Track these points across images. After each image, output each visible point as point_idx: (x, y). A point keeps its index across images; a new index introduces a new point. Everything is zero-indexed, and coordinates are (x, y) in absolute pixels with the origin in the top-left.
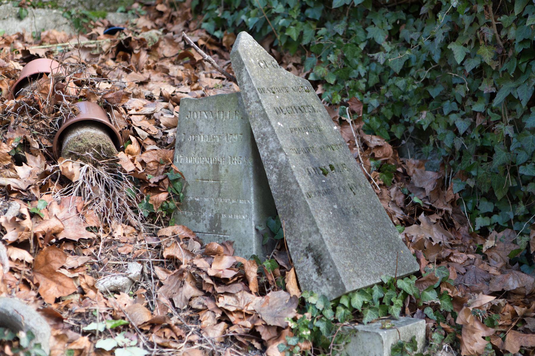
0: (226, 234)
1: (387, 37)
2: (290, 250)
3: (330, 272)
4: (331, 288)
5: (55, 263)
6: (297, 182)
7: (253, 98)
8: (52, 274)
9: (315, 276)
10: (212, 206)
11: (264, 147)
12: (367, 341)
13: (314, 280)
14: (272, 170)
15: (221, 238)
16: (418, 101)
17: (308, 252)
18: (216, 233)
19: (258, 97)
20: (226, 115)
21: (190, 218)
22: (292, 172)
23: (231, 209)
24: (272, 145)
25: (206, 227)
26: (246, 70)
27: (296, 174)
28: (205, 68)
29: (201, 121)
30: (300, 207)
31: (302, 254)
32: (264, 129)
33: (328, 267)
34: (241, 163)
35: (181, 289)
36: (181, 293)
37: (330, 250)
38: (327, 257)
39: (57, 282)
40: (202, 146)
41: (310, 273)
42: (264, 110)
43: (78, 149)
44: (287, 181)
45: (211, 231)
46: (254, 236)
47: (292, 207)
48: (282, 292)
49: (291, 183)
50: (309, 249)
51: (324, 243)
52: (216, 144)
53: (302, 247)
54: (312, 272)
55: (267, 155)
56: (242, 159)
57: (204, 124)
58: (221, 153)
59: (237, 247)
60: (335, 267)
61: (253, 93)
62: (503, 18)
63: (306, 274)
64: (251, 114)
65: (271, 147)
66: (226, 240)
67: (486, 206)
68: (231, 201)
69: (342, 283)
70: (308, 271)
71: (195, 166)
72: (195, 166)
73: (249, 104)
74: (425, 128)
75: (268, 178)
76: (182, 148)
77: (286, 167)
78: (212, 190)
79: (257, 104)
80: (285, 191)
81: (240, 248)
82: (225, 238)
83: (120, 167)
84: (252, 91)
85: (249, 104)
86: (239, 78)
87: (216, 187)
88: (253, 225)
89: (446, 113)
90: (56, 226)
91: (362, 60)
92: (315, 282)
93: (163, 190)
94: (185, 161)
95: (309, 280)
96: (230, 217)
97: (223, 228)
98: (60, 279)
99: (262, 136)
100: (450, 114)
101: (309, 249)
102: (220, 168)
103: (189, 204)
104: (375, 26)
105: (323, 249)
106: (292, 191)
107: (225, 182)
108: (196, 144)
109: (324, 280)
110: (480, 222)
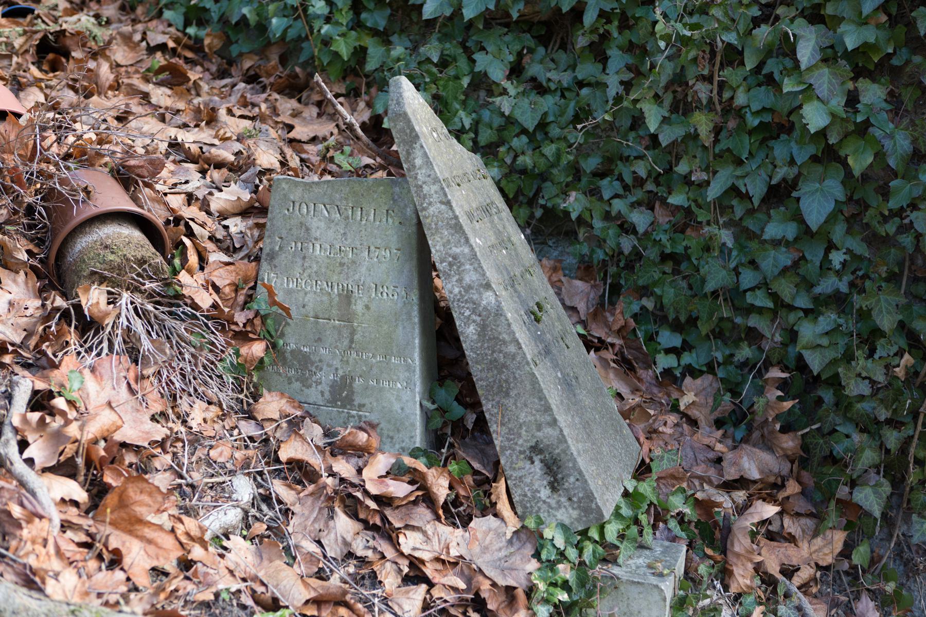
0: (364, 409)
1: (507, 73)
2: (498, 448)
3: (576, 488)
4: (575, 514)
5: (140, 506)
6: (517, 341)
7: (435, 196)
8: (132, 524)
9: (545, 493)
10: (336, 363)
11: (455, 279)
12: (637, 596)
13: (544, 498)
14: (468, 318)
15: (353, 417)
16: (568, 176)
17: (533, 454)
18: (345, 407)
19: (446, 195)
20: (368, 215)
21: (289, 379)
22: (509, 325)
23: (375, 370)
24: (470, 277)
25: (323, 396)
26: (422, 147)
27: (515, 327)
28: (201, 93)
29: (315, 219)
30: (522, 381)
31: (522, 456)
32: (454, 249)
33: (572, 479)
34: (396, 297)
35: (331, 523)
36: (334, 531)
37: (575, 453)
38: (571, 465)
39: (142, 538)
40: (318, 262)
41: (536, 486)
42: (456, 217)
43: (107, 267)
44: (498, 338)
45: (332, 402)
46: (418, 417)
47: (506, 381)
48: (490, 517)
49: (504, 342)
50: (536, 449)
51: (566, 442)
52: (346, 260)
53: (522, 446)
54: (540, 486)
55: (460, 292)
56: (398, 290)
57: (322, 225)
58: (357, 277)
59: (385, 432)
60: (586, 481)
61: (435, 188)
62: (727, 72)
63: (527, 489)
64: (428, 221)
65: (467, 279)
66: (364, 419)
67: (668, 339)
68: (374, 356)
69: (598, 507)
70: (532, 484)
71: (301, 294)
72: (301, 294)
73: (425, 205)
74: (574, 216)
75: (460, 329)
76: (276, 262)
77: (496, 315)
78: (336, 337)
79: (443, 207)
80: (492, 354)
81: (391, 434)
82: (360, 417)
83: (189, 301)
84: (434, 184)
85: (425, 205)
86: (407, 159)
87: (346, 333)
88: (418, 399)
89: (606, 196)
90: (113, 424)
91: (464, 103)
92: (544, 502)
93: (255, 337)
94: (282, 284)
95: (534, 497)
96: (372, 383)
97: (358, 400)
98: (148, 533)
99: (451, 259)
100: (612, 198)
101: (536, 449)
102: (353, 301)
103: (288, 355)
104: (487, 53)
105: (564, 451)
106: (506, 355)
107: (364, 326)
108: (304, 258)
109: (563, 499)
110: (664, 361)
